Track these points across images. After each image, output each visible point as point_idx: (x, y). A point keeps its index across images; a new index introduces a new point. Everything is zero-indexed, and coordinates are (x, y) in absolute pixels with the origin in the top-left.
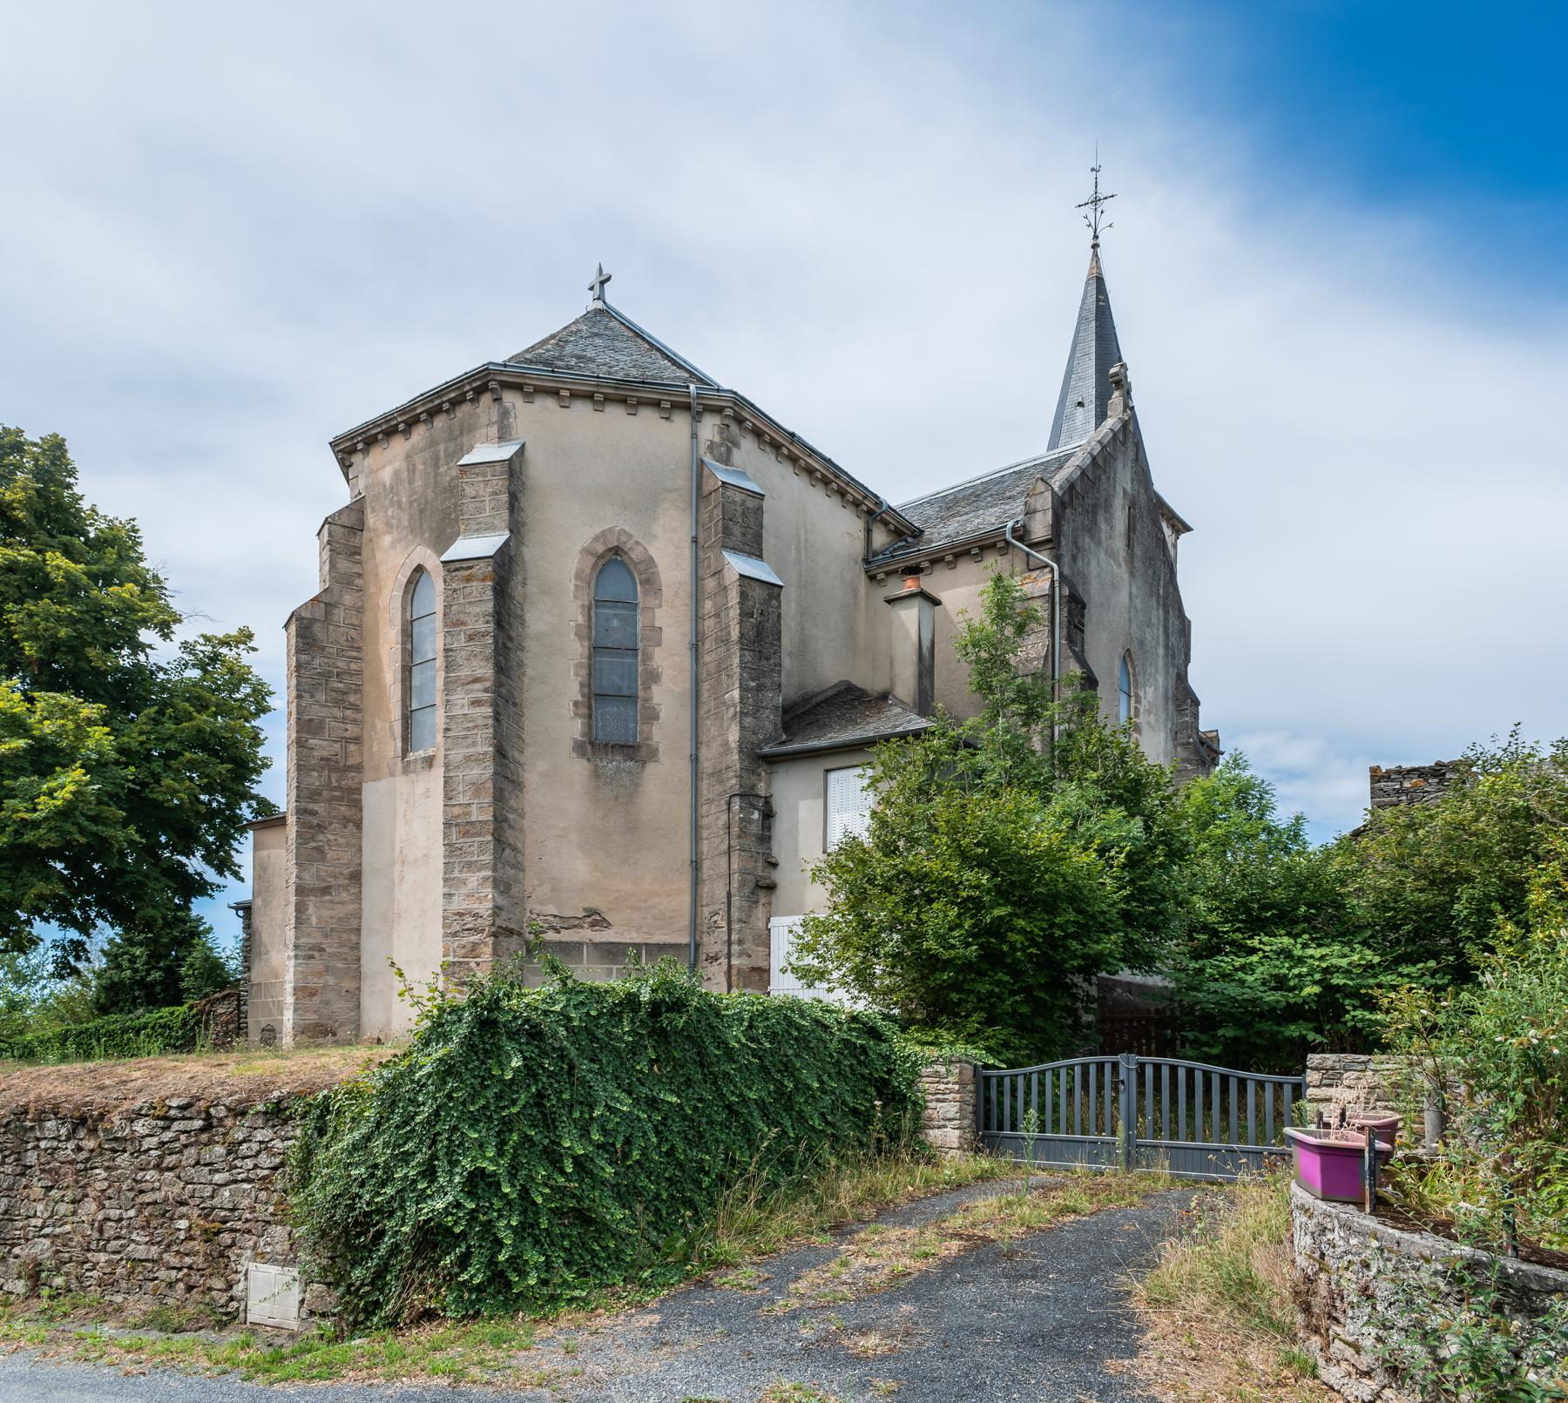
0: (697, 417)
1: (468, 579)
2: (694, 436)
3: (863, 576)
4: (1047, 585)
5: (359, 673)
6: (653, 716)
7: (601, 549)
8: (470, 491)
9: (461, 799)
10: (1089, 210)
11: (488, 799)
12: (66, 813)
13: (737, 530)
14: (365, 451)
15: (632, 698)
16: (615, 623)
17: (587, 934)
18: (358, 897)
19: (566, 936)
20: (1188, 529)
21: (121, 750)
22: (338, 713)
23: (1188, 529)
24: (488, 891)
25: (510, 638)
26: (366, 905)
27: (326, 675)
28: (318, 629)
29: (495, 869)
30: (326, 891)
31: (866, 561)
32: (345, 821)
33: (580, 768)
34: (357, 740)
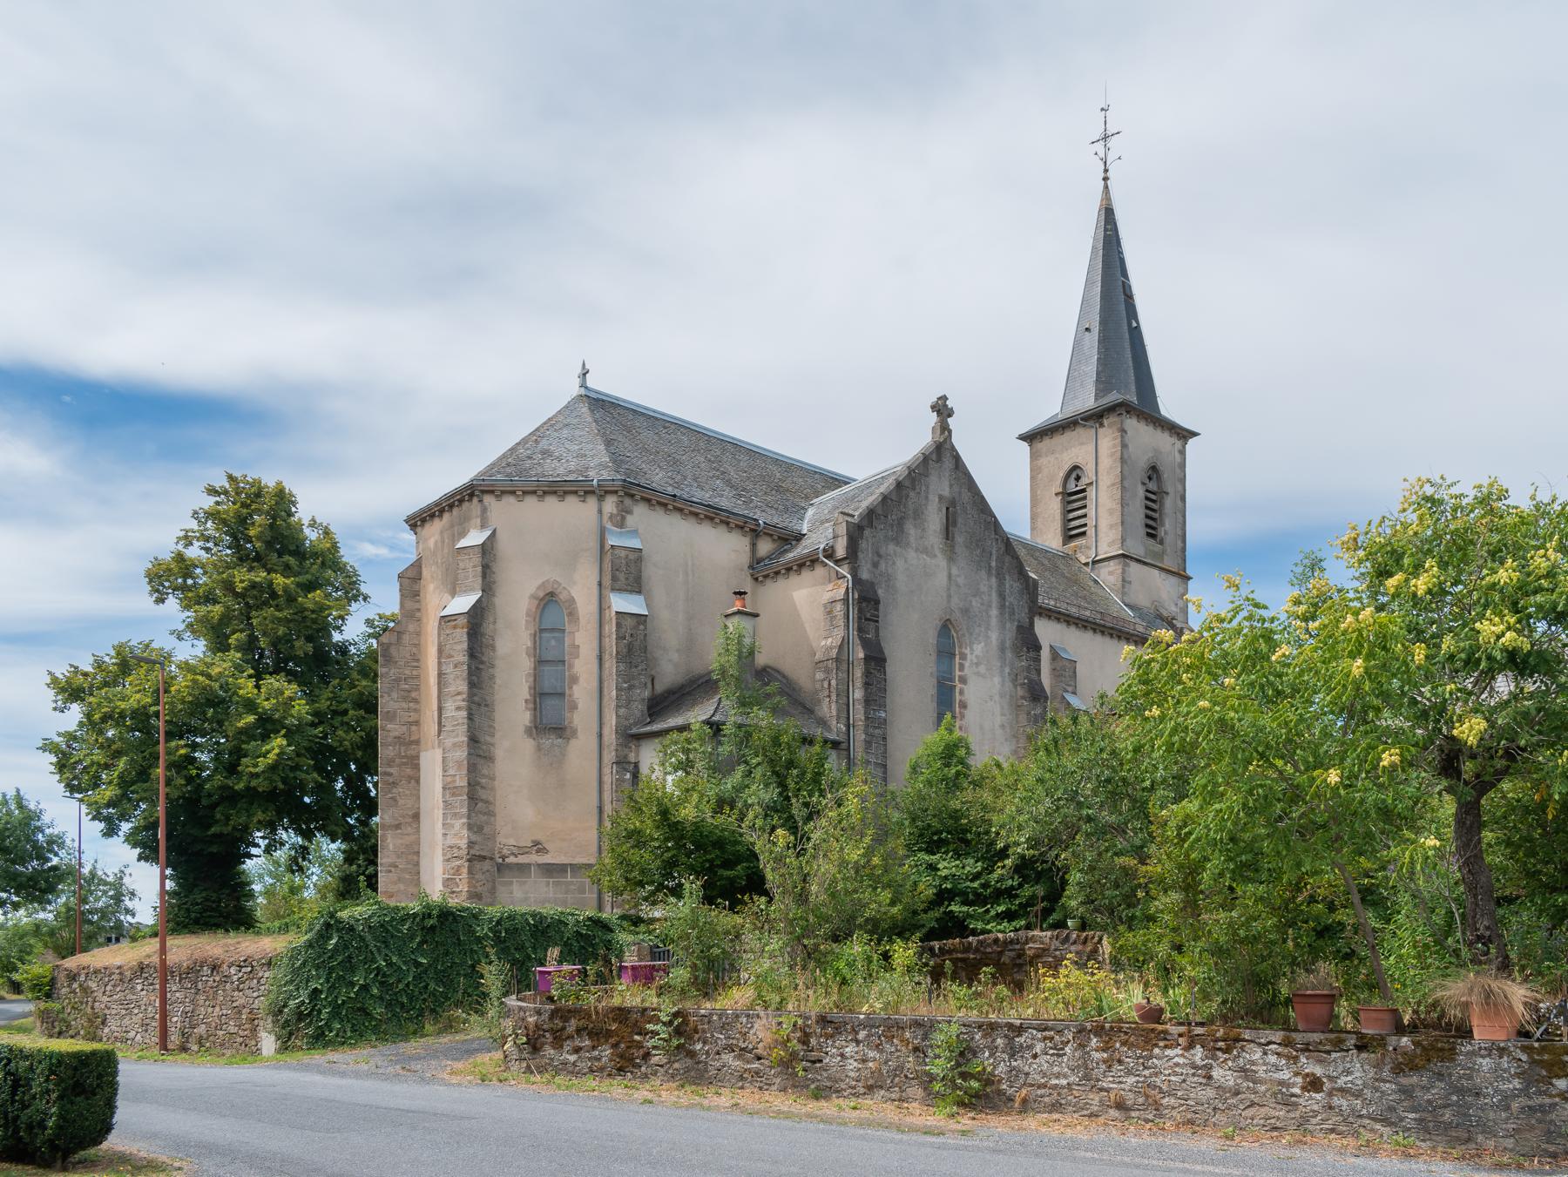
0: (601, 498)
1: (455, 627)
2: (600, 511)
3: (749, 579)
4: (843, 591)
5: (418, 677)
6: (574, 707)
7: (541, 594)
8: (461, 565)
9: (451, 772)
10: (1099, 147)
11: (465, 772)
12: (273, 768)
13: (622, 576)
14: (422, 525)
15: (562, 695)
16: (553, 643)
17: (534, 858)
18: (418, 830)
19: (522, 859)
20: (1194, 434)
21: (316, 714)
22: (404, 705)
23: (1194, 434)
24: (465, 832)
25: (482, 662)
26: (422, 834)
27: (398, 680)
28: (393, 651)
29: (469, 817)
30: (398, 827)
31: (751, 567)
32: (410, 778)
33: (528, 745)
34: (417, 723)
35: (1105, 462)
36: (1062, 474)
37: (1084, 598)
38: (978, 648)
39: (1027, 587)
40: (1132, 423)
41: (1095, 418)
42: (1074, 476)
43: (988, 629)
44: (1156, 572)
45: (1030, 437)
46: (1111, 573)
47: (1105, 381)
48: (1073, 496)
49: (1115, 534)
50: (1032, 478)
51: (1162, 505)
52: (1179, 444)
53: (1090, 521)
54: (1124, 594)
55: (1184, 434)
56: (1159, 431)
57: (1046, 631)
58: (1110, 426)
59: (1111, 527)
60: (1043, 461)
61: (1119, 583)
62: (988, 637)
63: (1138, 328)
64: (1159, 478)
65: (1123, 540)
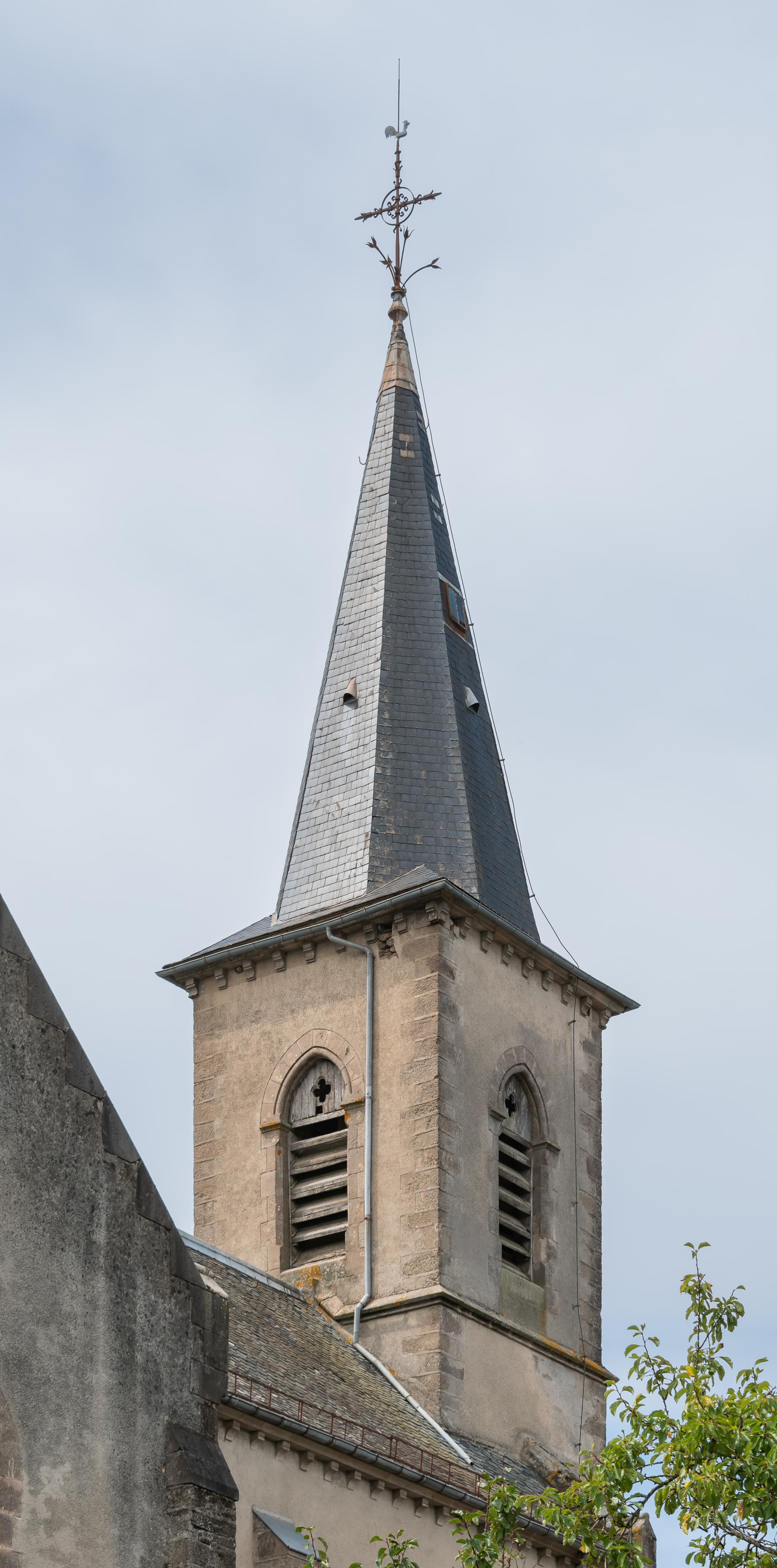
20: (624, 1004)
23: (624, 1004)
35: (397, 1049)
36: (279, 1077)
37: (343, 1400)
38: (55, 1479)
39: (197, 1318)
40: (464, 950)
41: (369, 927)
42: (312, 1082)
43: (82, 1424)
44: (526, 1354)
45: (195, 975)
46: (410, 1346)
47: (394, 834)
48: (311, 1138)
49: (424, 1241)
50: (200, 1084)
51: (541, 1179)
52: (584, 1026)
53: (356, 1206)
54: (444, 1402)
55: (601, 1003)
56: (535, 982)
57: (246, 1462)
58: (408, 953)
59: (412, 1221)
60: (229, 1040)
61: (433, 1375)
62: (81, 1448)
63: (480, 708)
64: (534, 1110)
65: (443, 1260)
